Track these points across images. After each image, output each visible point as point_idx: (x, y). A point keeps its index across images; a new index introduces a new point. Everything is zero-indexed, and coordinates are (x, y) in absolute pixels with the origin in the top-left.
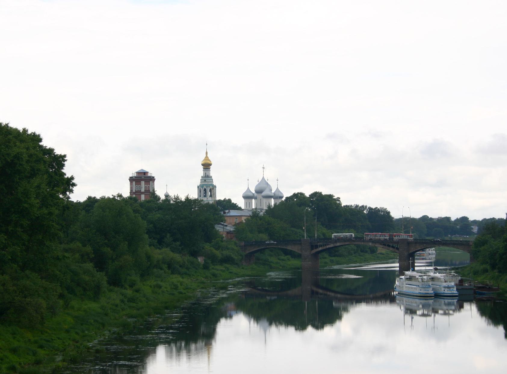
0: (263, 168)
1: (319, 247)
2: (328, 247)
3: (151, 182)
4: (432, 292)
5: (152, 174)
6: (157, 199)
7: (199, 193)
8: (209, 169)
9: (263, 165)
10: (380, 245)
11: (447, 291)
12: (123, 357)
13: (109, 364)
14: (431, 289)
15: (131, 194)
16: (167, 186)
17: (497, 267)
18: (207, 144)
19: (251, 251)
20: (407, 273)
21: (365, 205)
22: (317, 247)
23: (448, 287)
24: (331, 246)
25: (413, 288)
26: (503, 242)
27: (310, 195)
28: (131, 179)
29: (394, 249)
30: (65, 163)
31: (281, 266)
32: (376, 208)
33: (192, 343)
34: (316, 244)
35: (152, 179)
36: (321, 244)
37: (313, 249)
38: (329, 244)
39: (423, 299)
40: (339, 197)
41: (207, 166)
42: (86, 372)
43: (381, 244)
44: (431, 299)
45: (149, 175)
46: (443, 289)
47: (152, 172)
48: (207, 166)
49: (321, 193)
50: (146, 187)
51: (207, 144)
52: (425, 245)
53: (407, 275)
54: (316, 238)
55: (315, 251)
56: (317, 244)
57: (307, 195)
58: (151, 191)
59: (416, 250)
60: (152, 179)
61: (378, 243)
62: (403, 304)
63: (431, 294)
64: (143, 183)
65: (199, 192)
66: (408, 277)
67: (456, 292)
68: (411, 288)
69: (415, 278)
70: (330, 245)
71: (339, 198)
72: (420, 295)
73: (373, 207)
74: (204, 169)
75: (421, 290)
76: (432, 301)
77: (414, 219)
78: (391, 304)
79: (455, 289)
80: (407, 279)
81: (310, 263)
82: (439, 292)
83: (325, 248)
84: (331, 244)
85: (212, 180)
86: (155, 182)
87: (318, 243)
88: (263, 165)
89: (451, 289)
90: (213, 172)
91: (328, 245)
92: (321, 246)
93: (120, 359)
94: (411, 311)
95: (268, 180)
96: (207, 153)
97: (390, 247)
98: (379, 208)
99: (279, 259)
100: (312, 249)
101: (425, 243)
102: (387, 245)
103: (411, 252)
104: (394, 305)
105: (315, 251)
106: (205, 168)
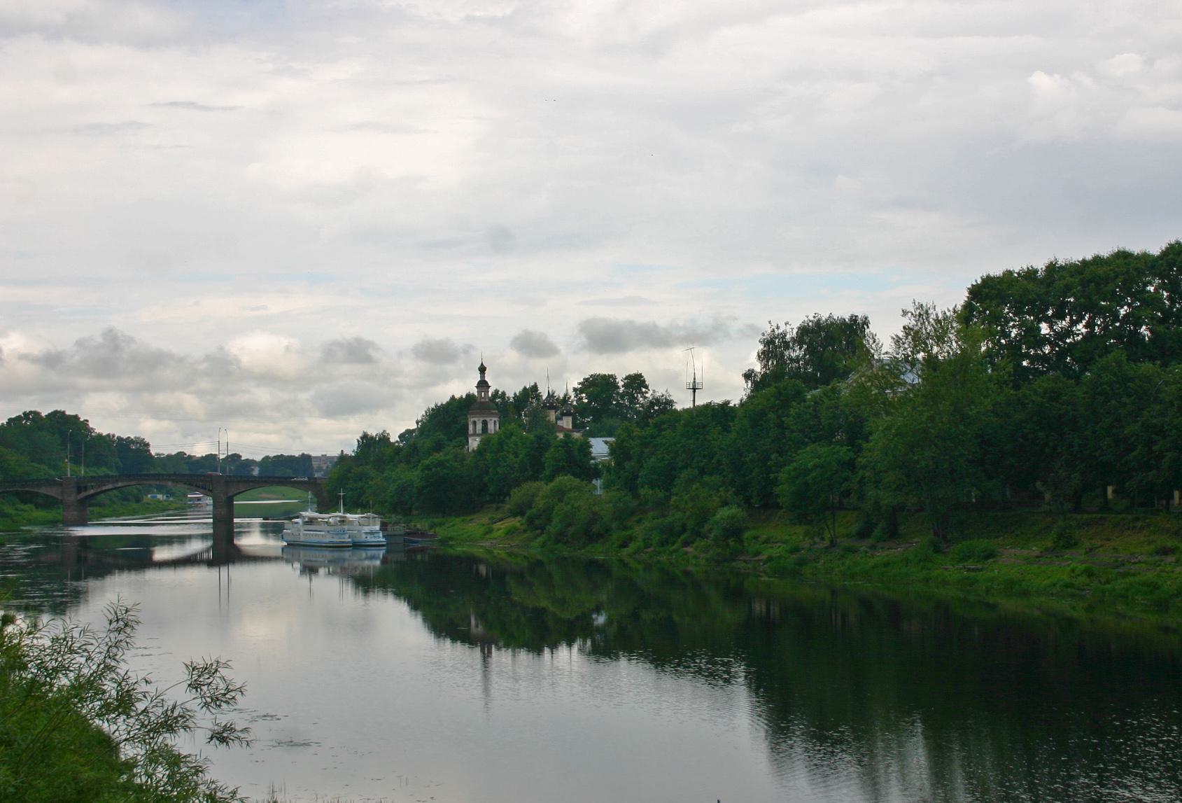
4: (350, 540)
11: (370, 539)
14: (347, 536)
17: (1136, 428)
20: (304, 513)
21: (112, 433)
22: (86, 488)
23: (371, 533)
25: (319, 535)
31: (24, 519)
32: (129, 438)
39: (337, 551)
40: (88, 419)
41: (482, 370)
44: (349, 551)
46: (364, 536)
48: (482, 370)
49: (64, 412)
52: (251, 484)
53: (304, 517)
55: (83, 495)
57: (44, 414)
61: (181, 482)
62: (299, 561)
63: (348, 542)
66: (306, 520)
67: (384, 540)
68: (316, 535)
69: (296, 525)
71: (87, 421)
72: (331, 545)
73: (125, 437)
75: (333, 538)
76: (350, 553)
78: (211, 568)
79: (381, 535)
80: (306, 522)
81: (75, 513)
82: (356, 540)
89: (376, 535)
91: (105, 485)
94: (310, 570)
98: (132, 437)
99: (16, 509)
100: (79, 491)
101: (252, 481)
103: (230, 494)
104: (246, 565)
105: (83, 495)
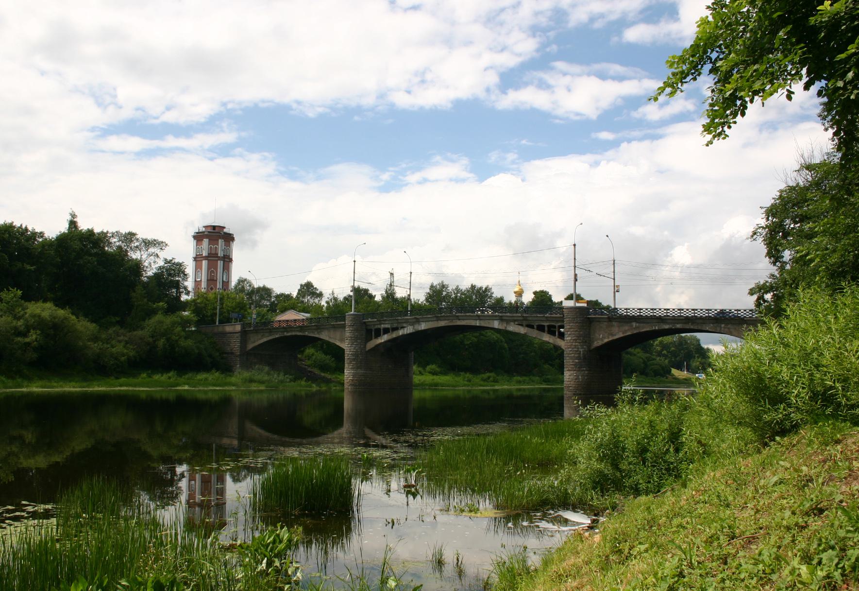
1: (384, 333)
6: (90, 317)
10: (520, 327)
12: (207, 473)
13: (47, 507)
30: (30, 229)
33: (450, 488)
34: (376, 327)
36: (387, 326)
37: (371, 339)
38: (405, 325)
42: (530, 319)
43: (522, 325)
52: (634, 324)
54: (820, 38)
56: (379, 326)
70: (406, 329)
84: (407, 327)
87: (381, 324)
91: (403, 327)
92: (386, 331)
93: (131, 545)
97: (534, 328)
102: (535, 327)
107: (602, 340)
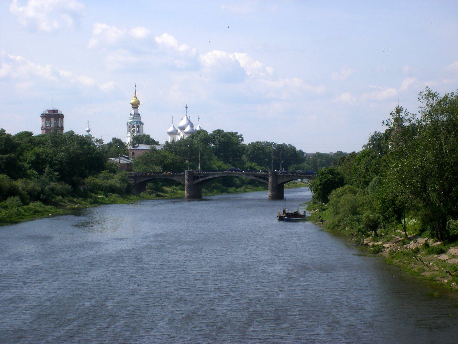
0: (186, 107)
2: (208, 178)
3: (59, 118)
5: (61, 111)
7: (128, 129)
8: (138, 107)
9: (186, 105)
15: (42, 129)
16: (88, 122)
18: (135, 86)
19: (141, 181)
24: (211, 178)
26: (101, 173)
27: (71, 133)
28: (43, 116)
29: (264, 180)
34: (197, 176)
35: (62, 116)
41: (136, 105)
45: (59, 113)
47: (62, 110)
48: (136, 105)
50: (55, 123)
51: (135, 86)
56: (198, 175)
58: (59, 127)
59: (284, 181)
60: (62, 116)
64: (52, 119)
65: (128, 128)
71: (242, 135)
74: (133, 107)
77: (321, 154)
83: (205, 179)
85: (140, 117)
86: (64, 119)
88: (186, 105)
90: (141, 110)
95: (190, 118)
96: (136, 94)
100: (194, 179)
103: (279, 183)
106: (134, 107)
107: (281, 182)
